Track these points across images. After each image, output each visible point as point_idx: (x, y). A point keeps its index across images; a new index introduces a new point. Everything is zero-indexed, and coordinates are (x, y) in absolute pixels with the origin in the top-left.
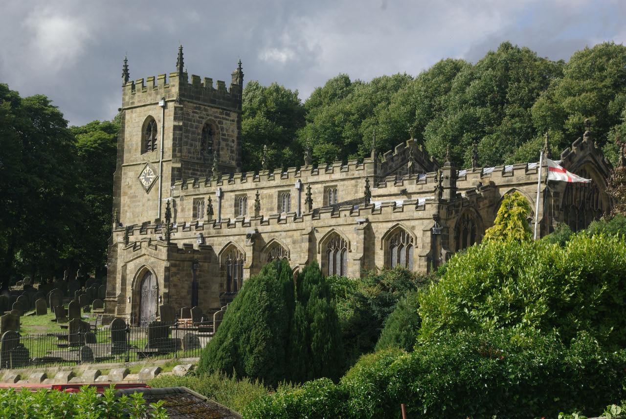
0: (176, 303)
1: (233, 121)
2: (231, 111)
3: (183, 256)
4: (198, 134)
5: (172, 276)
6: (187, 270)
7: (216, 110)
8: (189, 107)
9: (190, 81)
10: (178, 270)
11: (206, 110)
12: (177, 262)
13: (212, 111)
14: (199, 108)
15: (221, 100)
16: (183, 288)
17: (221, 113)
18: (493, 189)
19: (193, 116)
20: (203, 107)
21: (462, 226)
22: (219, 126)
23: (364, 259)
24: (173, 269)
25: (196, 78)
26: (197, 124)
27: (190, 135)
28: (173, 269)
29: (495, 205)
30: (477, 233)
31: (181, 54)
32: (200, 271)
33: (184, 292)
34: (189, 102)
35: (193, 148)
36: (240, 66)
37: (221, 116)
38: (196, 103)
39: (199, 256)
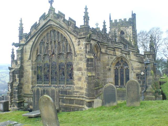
9: (113, 22)
17: (125, 28)
25: (116, 21)
31: (110, 15)
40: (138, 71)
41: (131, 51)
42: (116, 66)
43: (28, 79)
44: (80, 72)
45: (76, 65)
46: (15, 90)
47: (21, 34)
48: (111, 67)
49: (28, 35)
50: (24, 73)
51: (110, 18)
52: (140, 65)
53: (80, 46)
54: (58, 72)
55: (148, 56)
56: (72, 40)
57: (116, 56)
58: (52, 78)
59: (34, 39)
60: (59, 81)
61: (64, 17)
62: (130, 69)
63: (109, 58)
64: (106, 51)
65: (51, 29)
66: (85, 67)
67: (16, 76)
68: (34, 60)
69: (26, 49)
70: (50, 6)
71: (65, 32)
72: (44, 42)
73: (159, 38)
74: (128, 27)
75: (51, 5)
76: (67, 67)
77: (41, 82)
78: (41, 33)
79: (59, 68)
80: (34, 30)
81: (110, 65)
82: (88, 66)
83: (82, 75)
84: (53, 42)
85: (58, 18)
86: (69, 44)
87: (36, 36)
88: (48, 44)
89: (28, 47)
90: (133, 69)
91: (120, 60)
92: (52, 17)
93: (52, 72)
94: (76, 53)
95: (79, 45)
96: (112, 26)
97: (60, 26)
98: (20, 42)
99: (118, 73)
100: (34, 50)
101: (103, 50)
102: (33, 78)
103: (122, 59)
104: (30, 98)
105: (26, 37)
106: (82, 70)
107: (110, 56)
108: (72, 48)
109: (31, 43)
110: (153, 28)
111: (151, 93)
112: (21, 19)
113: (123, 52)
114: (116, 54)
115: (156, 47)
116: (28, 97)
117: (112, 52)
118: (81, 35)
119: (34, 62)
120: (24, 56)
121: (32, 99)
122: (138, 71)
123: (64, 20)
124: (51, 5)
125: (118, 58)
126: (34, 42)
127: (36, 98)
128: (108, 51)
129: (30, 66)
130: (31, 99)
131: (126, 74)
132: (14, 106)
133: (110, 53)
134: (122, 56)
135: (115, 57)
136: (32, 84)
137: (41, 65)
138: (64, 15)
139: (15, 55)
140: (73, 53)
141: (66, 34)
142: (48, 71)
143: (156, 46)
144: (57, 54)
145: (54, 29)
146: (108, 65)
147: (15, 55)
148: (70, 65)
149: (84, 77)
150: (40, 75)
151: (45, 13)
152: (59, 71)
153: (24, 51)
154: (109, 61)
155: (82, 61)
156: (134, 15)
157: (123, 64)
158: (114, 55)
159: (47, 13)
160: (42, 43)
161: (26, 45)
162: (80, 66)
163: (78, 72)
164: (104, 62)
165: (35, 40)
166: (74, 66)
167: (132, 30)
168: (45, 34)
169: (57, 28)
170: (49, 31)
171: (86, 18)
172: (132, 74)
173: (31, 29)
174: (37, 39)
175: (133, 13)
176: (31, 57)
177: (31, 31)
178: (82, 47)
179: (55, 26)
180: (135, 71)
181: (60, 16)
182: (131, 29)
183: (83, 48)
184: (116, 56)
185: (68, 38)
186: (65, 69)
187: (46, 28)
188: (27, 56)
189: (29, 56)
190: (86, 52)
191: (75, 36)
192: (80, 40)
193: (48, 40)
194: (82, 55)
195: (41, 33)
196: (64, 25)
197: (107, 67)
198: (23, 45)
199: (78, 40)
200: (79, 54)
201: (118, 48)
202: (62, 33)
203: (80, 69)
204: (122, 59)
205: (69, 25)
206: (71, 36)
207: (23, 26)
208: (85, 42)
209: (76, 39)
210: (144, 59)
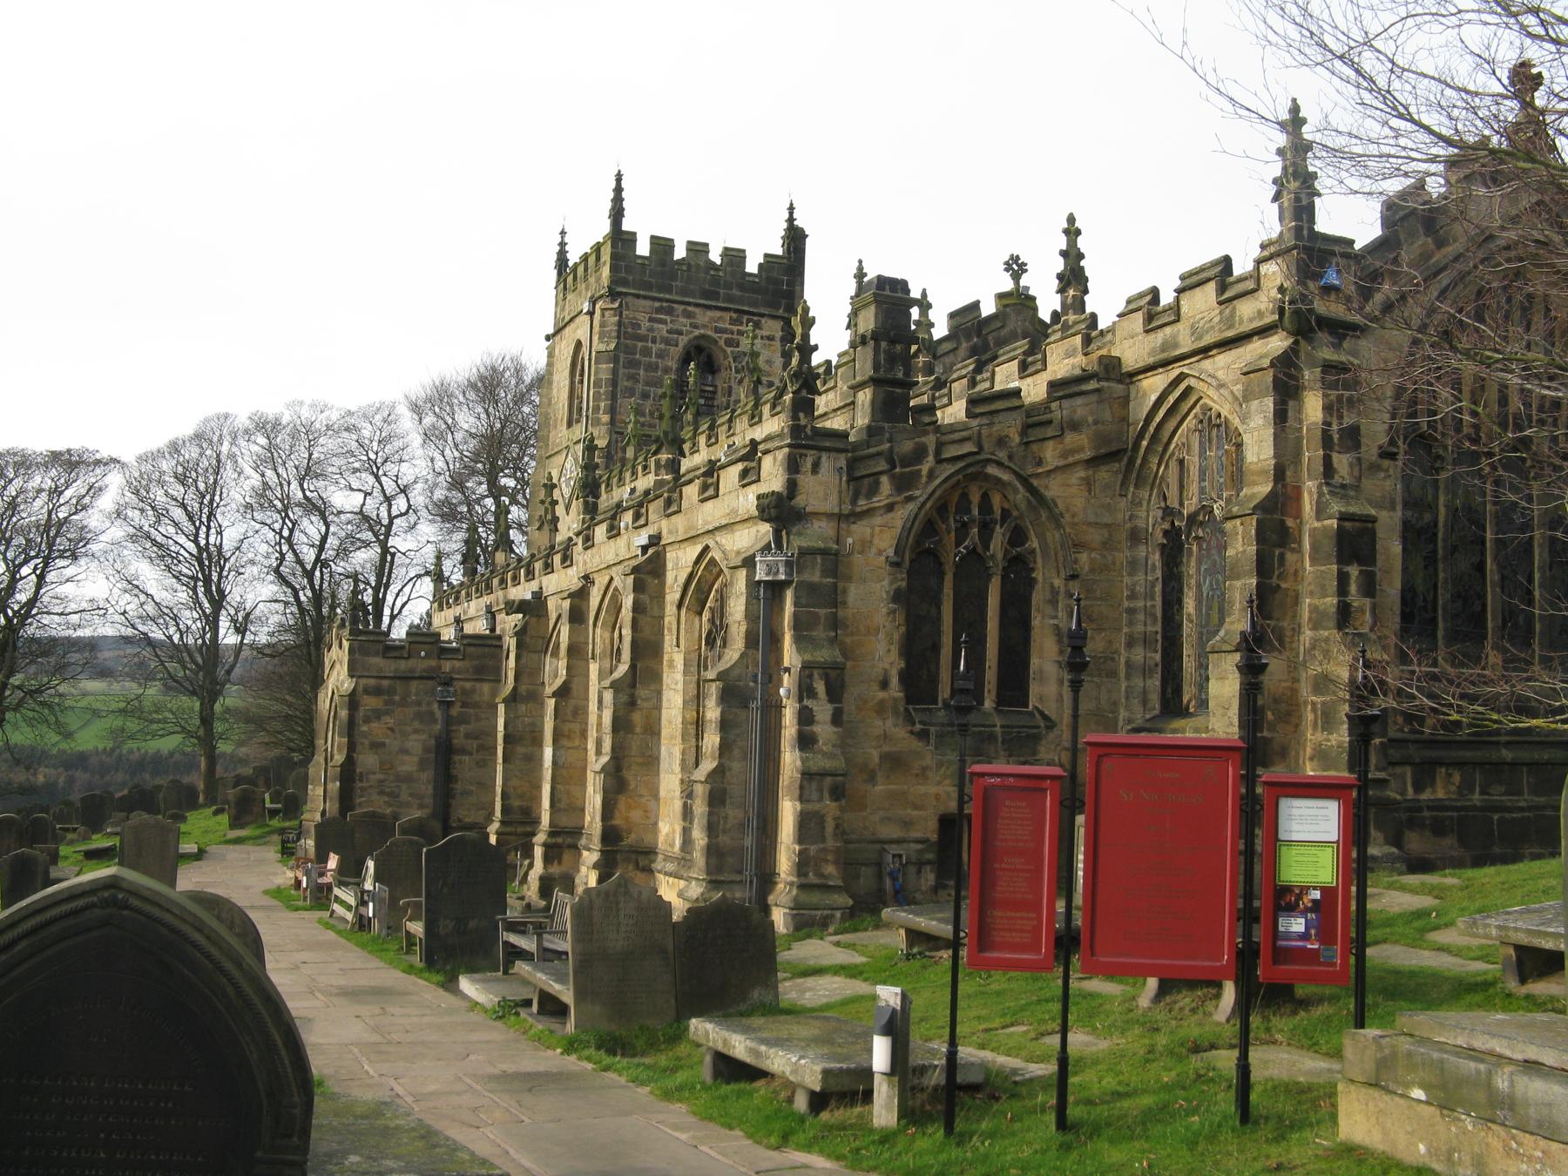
0: (382, 793)
1: (771, 338)
2: (763, 315)
3: (403, 665)
4: (667, 370)
5: (367, 720)
6: (419, 704)
7: (718, 314)
8: (641, 312)
9: (643, 249)
10: (386, 703)
11: (689, 315)
12: (385, 683)
13: (703, 317)
14: (670, 312)
15: (736, 292)
16: (405, 751)
17: (733, 322)
18: (1119, 388)
19: (651, 330)
20: (680, 308)
21: (952, 554)
22: (729, 350)
23: (633, 686)
24: (370, 703)
25: (662, 245)
26: (662, 346)
27: (642, 372)
28: (370, 703)
29: (1129, 453)
30: (1038, 575)
31: (618, 190)
32: (464, 705)
33: (408, 765)
34: (638, 296)
35: (650, 402)
36: (791, 214)
37: (735, 328)
38: (660, 300)
39: (457, 664)
51: (617, 213)
96: (625, 283)
121: (1409, 775)
149: (158, 781)
150: (1420, 589)
156: (795, 238)
171: (1073, 278)
182: (777, 344)
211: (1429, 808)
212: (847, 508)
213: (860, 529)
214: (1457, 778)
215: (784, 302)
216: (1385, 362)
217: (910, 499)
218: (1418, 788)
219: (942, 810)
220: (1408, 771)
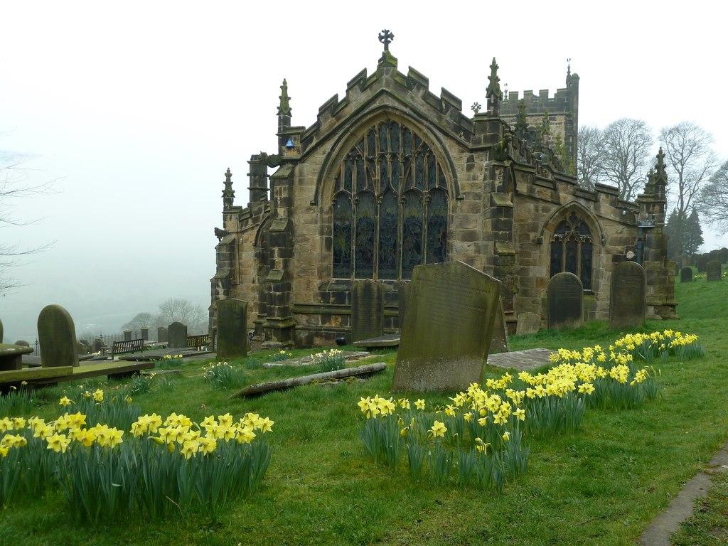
2: (556, 115)
40: (619, 248)
41: (603, 192)
42: (555, 233)
43: (310, 263)
44: (471, 243)
45: (461, 225)
46: (272, 292)
47: (285, 129)
48: (542, 234)
49: (310, 132)
50: (297, 246)
52: (625, 233)
53: (475, 171)
54: (401, 243)
55: (648, 208)
56: (451, 154)
57: (559, 204)
58: (381, 261)
59: (328, 146)
60: (403, 268)
61: (427, 88)
62: (596, 242)
63: (537, 211)
64: (531, 190)
65: (383, 119)
66: (489, 230)
67: (273, 252)
68: (326, 209)
69: (301, 173)
70: (383, 50)
71: (429, 129)
72: (359, 156)
73: (637, 159)
74: (554, 119)
75: (386, 48)
76: (428, 229)
77: (345, 270)
78: (352, 130)
79: (404, 232)
80: (331, 119)
81: (540, 230)
82: (496, 226)
83: (478, 251)
84: (388, 156)
85: (410, 88)
86: (438, 164)
87: (336, 138)
88: (371, 161)
89: (310, 169)
90: (603, 244)
91: (568, 215)
92: (388, 84)
93: (381, 243)
94: (461, 191)
95: (470, 168)
97: (415, 112)
98: (280, 150)
99: (561, 254)
100: (329, 173)
101: (523, 188)
102: (324, 258)
103: (573, 213)
104: (316, 316)
105: (305, 139)
106: (478, 240)
107: (541, 205)
108: (448, 176)
109: (319, 157)
110: (622, 123)
111: (653, 307)
112: (285, 83)
113: (578, 194)
114: (558, 197)
115: (625, 188)
116: (307, 314)
117: (549, 192)
118: (478, 142)
119: (327, 213)
120: (296, 194)
122: (619, 248)
123: (428, 96)
124: (386, 48)
125: (564, 211)
126: (329, 155)
127: (361, 309)
128: (538, 189)
129: (316, 222)
130: (318, 319)
131: (583, 254)
132: (268, 339)
133: (544, 198)
134: (574, 205)
135: (554, 208)
136: (320, 277)
137: (347, 223)
138: (426, 81)
139: (234, 191)
140: (450, 192)
141: (433, 138)
142: (371, 240)
143: (625, 184)
144: (399, 192)
145: (393, 119)
146: (534, 229)
147: (234, 191)
148: (439, 226)
150: (344, 249)
151: (365, 70)
152: (404, 240)
153: (296, 180)
154: (537, 218)
155: (477, 215)
156: (573, 81)
157: (577, 227)
158: (554, 203)
159: (372, 70)
160: (354, 159)
161: (303, 162)
162: (471, 227)
163: (466, 244)
164: (521, 220)
165: (333, 149)
166: (453, 227)
167: (566, 129)
168: (365, 131)
169: (406, 117)
170: (376, 123)
172: (603, 255)
173: (318, 116)
174: (340, 145)
175: (571, 74)
176: (319, 197)
177: (318, 119)
178: (478, 174)
179: (397, 110)
180: (609, 247)
181: (416, 81)
182: (563, 125)
183: (481, 177)
184: (559, 204)
185: (437, 148)
186: (425, 235)
187: (369, 117)
188: (305, 194)
189: (314, 193)
190: (493, 190)
191: (459, 143)
192: (472, 156)
193: (372, 151)
194: (478, 196)
195: (352, 130)
196: (423, 109)
197: (532, 235)
198: (295, 162)
199: (467, 154)
200: (469, 193)
201: (564, 181)
202: (417, 132)
203: (470, 236)
204: (573, 213)
205: (441, 111)
206: (447, 143)
207: (291, 103)
208: (487, 162)
209: (463, 152)
210: (636, 215)
211: (325, 330)
212: (239, 230)
213: (245, 236)
214: (340, 319)
215: (565, 107)
216: (314, 170)
217: (257, 225)
218: (323, 322)
219: (160, 326)
220: (320, 317)
